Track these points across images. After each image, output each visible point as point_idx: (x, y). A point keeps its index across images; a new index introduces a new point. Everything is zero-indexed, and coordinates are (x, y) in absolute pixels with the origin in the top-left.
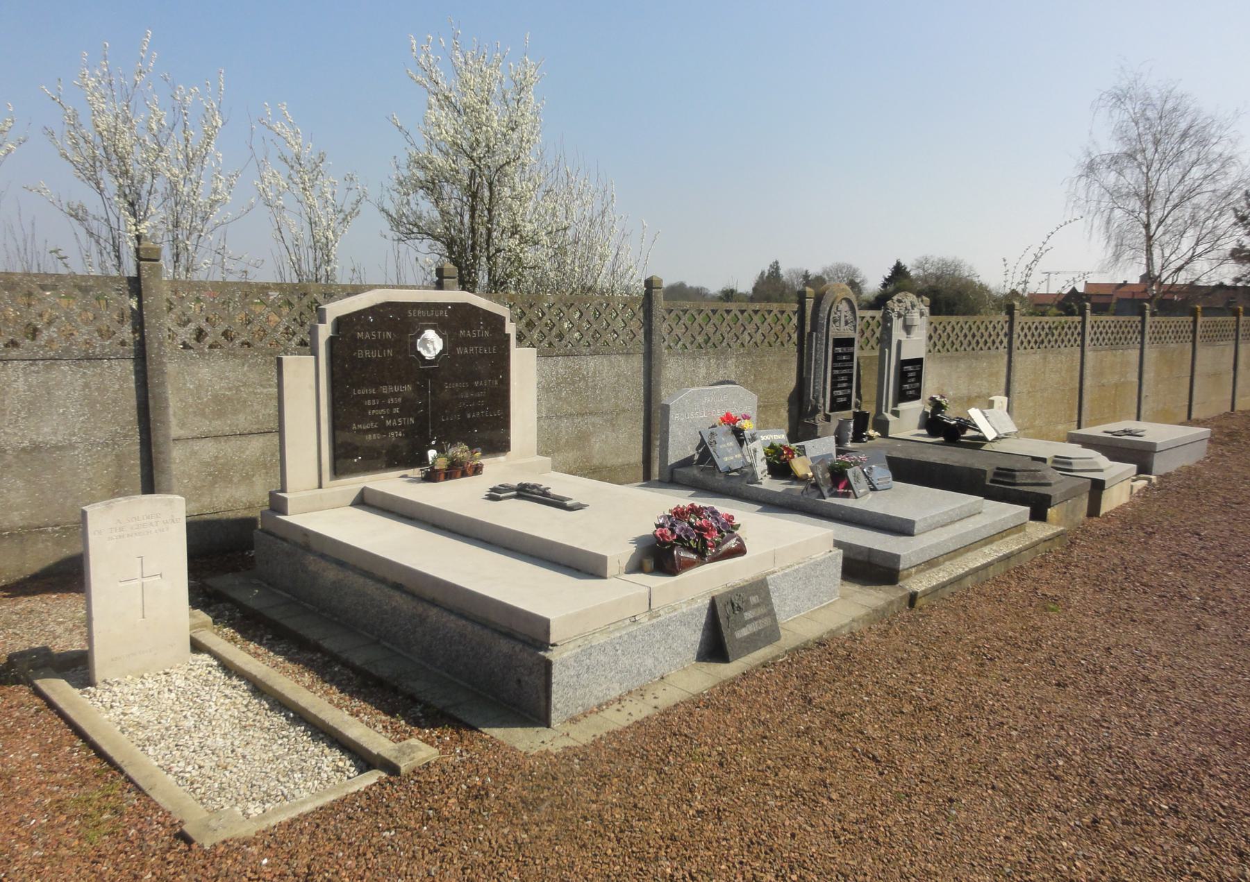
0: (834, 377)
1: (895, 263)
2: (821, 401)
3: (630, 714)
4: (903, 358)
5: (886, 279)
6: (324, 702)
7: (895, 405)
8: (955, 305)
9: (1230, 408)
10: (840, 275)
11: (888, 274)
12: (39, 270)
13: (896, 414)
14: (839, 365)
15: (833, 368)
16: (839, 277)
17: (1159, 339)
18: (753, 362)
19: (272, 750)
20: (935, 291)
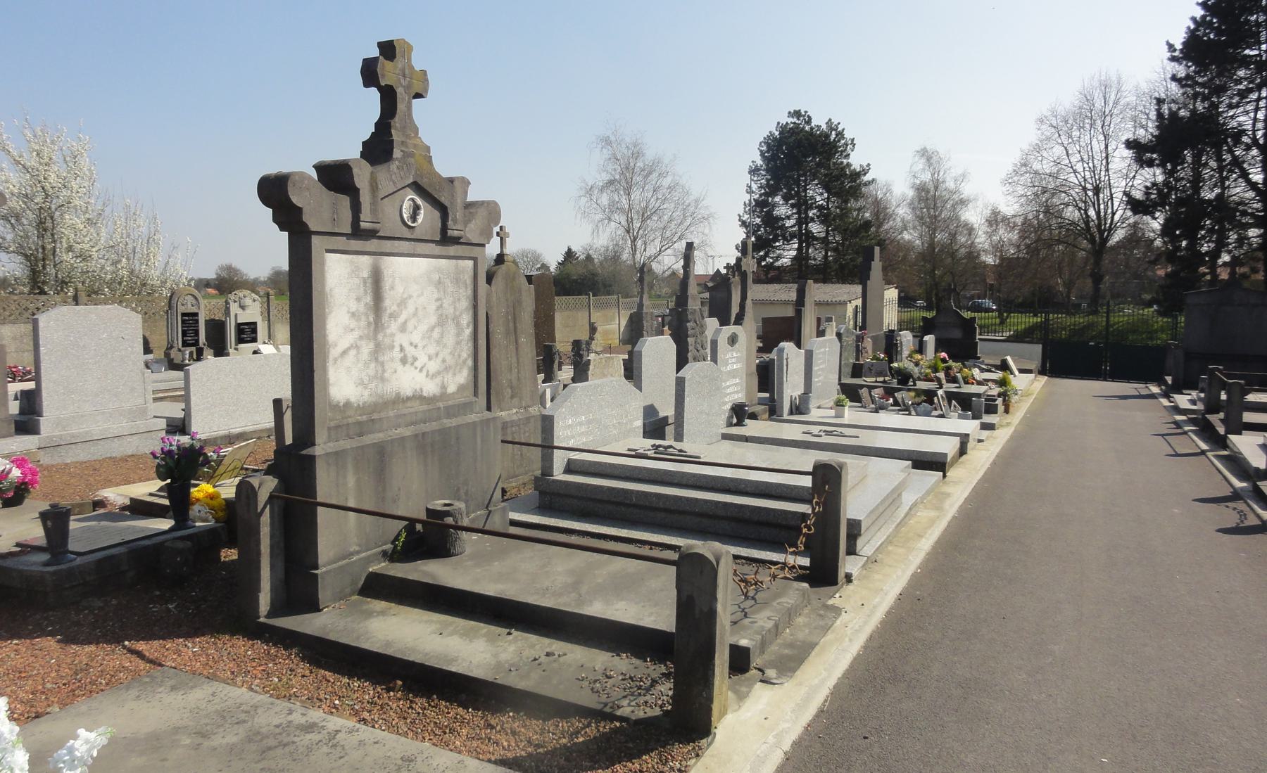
0: (183, 331)
1: (566, 250)
2: (176, 342)
3: (765, 719)
4: (239, 322)
5: (559, 263)
6: (176, 699)
7: (236, 345)
8: (610, 286)
9: (41, 324)
10: (525, 259)
11: (561, 259)
12: (483, 527)
13: (236, 349)
14: (184, 325)
15: (182, 327)
16: (524, 262)
17: (596, 307)
18: (148, 325)
19: (43, 687)
20: (593, 274)
